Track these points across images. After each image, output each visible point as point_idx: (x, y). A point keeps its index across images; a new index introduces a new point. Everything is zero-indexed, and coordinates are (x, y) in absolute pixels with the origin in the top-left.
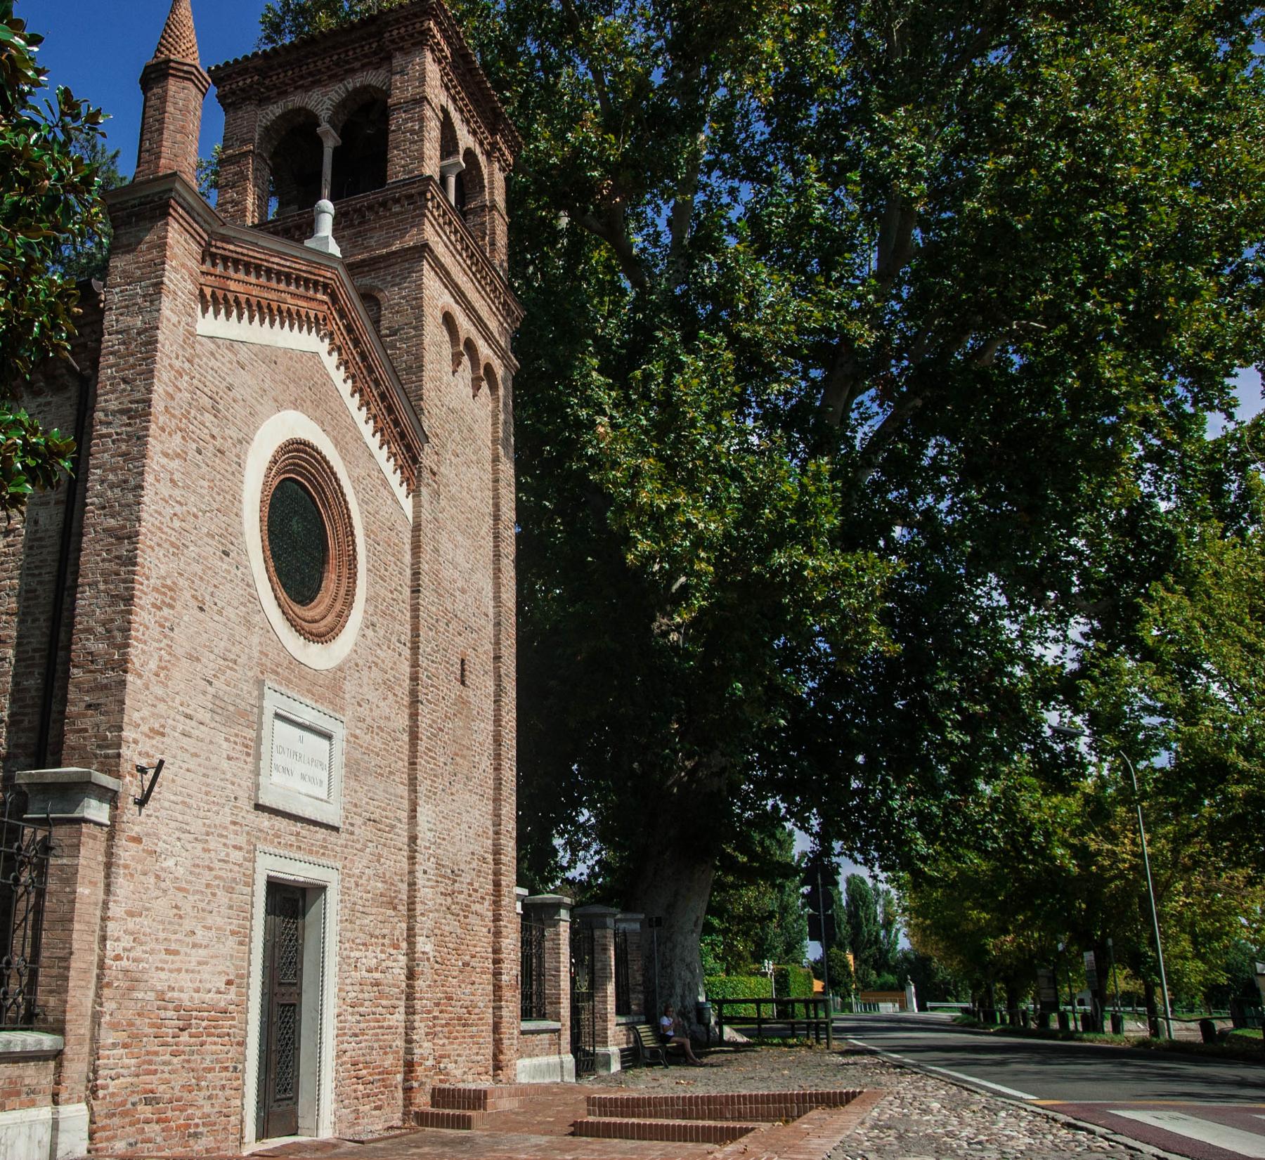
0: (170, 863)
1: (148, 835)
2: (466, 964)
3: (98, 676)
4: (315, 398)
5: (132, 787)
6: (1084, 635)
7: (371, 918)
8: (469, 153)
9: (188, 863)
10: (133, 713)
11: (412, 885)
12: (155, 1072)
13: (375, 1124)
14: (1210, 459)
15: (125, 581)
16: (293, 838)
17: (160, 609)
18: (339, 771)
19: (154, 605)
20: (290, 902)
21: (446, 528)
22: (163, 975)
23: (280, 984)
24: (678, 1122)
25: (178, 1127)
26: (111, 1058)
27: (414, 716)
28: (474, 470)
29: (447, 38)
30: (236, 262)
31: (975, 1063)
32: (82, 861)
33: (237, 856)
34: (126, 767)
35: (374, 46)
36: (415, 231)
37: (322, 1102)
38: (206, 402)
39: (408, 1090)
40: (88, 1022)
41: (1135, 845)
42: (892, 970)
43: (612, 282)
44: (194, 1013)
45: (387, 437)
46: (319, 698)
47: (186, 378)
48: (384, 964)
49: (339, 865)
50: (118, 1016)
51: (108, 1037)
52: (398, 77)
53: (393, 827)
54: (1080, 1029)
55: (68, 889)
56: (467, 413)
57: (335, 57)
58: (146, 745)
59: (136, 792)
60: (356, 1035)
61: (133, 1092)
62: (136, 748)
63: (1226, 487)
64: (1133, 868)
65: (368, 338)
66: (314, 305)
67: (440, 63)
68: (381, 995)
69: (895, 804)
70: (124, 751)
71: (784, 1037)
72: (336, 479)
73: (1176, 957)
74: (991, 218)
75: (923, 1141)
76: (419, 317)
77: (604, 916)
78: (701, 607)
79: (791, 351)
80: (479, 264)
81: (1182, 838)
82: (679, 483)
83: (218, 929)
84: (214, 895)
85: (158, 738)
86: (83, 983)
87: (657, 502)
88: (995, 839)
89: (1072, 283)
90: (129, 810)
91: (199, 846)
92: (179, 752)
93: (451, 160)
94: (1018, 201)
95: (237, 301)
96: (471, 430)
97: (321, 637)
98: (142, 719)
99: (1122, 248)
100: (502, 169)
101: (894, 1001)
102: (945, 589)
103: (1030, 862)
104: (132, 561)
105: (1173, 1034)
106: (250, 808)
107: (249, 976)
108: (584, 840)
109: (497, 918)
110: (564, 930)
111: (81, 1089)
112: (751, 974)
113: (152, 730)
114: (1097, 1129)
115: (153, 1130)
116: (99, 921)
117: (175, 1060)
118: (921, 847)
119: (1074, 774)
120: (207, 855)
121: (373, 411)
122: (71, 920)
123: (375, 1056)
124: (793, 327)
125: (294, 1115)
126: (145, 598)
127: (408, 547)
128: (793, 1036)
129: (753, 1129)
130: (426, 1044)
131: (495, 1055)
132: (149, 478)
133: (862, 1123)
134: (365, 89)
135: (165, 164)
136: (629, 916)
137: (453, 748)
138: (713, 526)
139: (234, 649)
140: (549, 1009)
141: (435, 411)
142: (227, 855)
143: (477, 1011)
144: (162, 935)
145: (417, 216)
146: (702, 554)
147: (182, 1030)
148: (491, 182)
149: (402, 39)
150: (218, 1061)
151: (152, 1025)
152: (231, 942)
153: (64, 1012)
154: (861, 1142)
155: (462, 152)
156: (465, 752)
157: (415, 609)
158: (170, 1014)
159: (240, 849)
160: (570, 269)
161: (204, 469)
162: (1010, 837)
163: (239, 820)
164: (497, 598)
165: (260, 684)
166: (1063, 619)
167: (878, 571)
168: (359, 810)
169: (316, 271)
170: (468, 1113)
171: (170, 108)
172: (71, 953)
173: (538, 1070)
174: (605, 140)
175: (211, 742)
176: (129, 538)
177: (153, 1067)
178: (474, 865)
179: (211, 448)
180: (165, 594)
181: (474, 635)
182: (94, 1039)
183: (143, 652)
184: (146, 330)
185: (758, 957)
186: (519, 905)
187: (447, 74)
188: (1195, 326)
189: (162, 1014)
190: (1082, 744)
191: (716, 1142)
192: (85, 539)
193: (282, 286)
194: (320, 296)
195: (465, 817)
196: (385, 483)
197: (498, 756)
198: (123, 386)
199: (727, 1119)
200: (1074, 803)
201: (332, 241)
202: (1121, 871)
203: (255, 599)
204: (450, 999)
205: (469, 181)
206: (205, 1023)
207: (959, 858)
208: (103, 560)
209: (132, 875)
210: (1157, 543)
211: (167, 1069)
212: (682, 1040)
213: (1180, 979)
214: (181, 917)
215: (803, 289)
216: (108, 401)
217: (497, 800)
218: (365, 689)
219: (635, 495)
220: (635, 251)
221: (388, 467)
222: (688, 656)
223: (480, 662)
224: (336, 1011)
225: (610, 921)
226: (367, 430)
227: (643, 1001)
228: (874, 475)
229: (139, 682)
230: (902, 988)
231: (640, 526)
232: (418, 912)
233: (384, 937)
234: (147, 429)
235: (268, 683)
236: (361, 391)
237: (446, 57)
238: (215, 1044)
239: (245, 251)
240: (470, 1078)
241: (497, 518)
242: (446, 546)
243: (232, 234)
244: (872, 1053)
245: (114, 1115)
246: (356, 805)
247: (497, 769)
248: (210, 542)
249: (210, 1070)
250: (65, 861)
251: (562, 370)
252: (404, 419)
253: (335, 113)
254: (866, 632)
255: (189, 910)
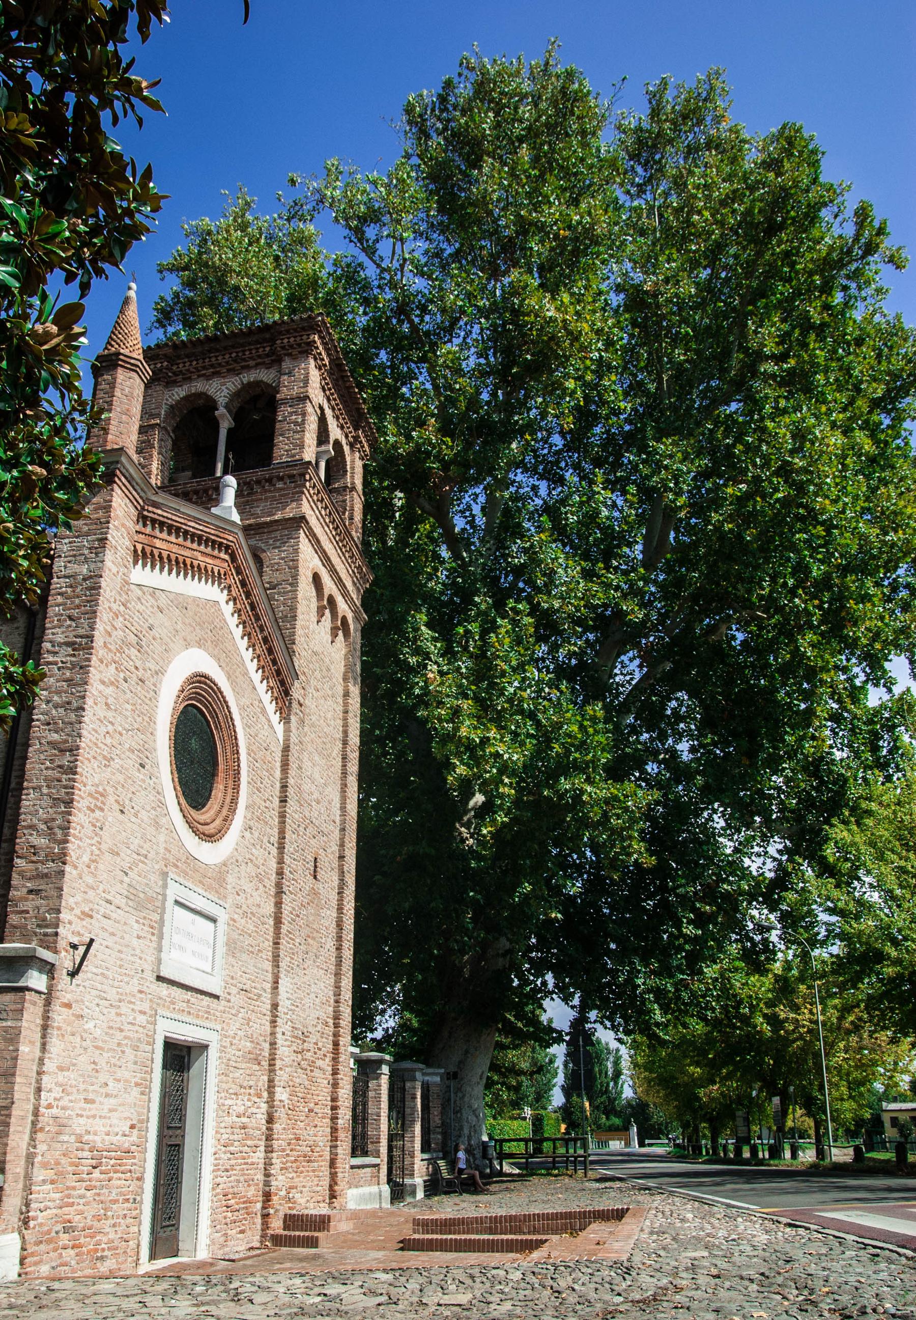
0: (90, 1025)
1: (77, 1001)
2: (310, 1111)
3: (39, 865)
4: (213, 640)
5: (65, 960)
6: (779, 851)
7: (241, 1071)
8: (337, 443)
9: (105, 1025)
10: (68, 900)
11: (273, 1044)
12: (72, 1205)
13: (239, 1246)
14: (870, 722)
15: (66, 787)
16: (185, 1005)
17: (93, 811)
18: (221, 949)
19: (89, 808)
20: (180, 1057)
21: (307, 751)
22: (82, 1121)
23: (169, 1128)
24: (486, 1237)
25: (89, 1252)
26: (44, 1194)
27: (278, 904)
28: (330, 703)
29: (327, 350)
30: (162, 524)
31: (701, 1184)
32: (24, 1024)
33: (142, 1019)
34: (62, 944)
35: (268, 349)
36: (294, 505)
37: (200, 1227)
38: (132, 639)
39: (265, 1216)
40: (23, 1162)
41: (812, 1013)
42: (618, 1114)
43: (434, 552)
44: (105, 1153)
45: (267, 674)
46: (209, 888)
47: (121, 619)
48: (250, 1111)
49: (219, 1027)
50: (48, 1157)
51: (39, 1174)
52: (286, 377)
53: (259, 996)
54: (767, 1156)
55: (11, 1048)
56: (326, 654)
57: (234, 355)
58: (78, 926)
59: (69, 965)
60: (227, 1171)
61: (57, 1222)
62: (70, 929)
63: (881, 743)
64: (810, 1031)
65: (257, 592)
66: (217, 562)
67: (320, 369)
68: (248, 1137)
69: (639, 981)
70: (60, 930)
71: (547, 1169)
72: (228, 707)
73: (837, 1099)
74: (731, 531)
75: (693, 1241)
76: (295, 577)
77: (414, 1070)
78: (503, 822)
79: (579, 622)
80: (341, 533)
81: (846, 1010)
82: (491, 720)
83: (126, 1081)
84: (123, 1052)
85: (88, 919)
86: (20, 1129)
87: (472, 736)
88: (713, 1010)
89: (785, 584)
90: (63, 979)
91: (113, 1011)
92: (101, 932)
93: (323, 448)
94: (749, 519)
95: (160, 556)
96: (328, 670)
97: (210, 837)
98: (76, 903)
99: (819, 560)
100: (362, 458)
101: (620, 1139)
102: (680, 812)
103: (738, 1028)
104: (72, 770)
105: (834, 1159)
106: (153, 979)
107: (148, 1121)
108: (381, 1006)
109: (335, 1072)
110: (384, 1081)
111: (15, 1221)
112: (513, 1118)
113: (83, 913)
114: (812, 1226)
115: (69, 1255)
116: (35, 1075)
117: (88, 1194)
118: (658, 1016)
119: (767, 959)
120: (119, 1019)
121: (258, 652)
122: (14, 1075)
123: (241, 1188)
124: (582, 603)
125: (175, 1239)
126: (82, 802)
127: (278, 764)
128: (555, 1168)
129: (546, 1241)
130: (280, 1178)
131: (331, 1186)
132: (89, 701)
133: (642, 1230)
134: (258, 383)
135: (113, 440)
136: (431, 1070)
137: (307, 931)
138: (515, 757)
139: (145, 846)
140: (370, 1147)
141: (303, 653)
142: (135, 1019)
143: (318, 1149)
144: (82, 1087)
145: (297, 493)
146: (506, 780)
147: (94, 1168)
148: (353, 468)
149: (291, 347)
150: (122, 1194)
151: (72, 1164)
152: (135, 1092)
153: (5, 1153)
154: (649, 1244)
155: (332, 442)
156: (315, 934)
157: (282, 816)
158: (86, 1154)
159: (145, 1013)
160: (402, 541)
161: (129, 695)
162: (725, 1008)
163: (145, 989)
164: (343, 808)
165: (165, 875)
166: (765, 838)
167: (638, 796)
168: (234, 982)
169: (222, 535)
170: (316, 1234)
171: (118, 393)
172: (13, 1103)
173: (362, 1198)
174: (444, 443)
175: (125, 923)
176: (71, 751)
177: (71, 1200)
178: (319, 1028)
179: (135, 678)
180: (97, 799)
181: (325, 838)
182: (28, 1177)
183: (79, 847)
184: (91, 577)
185: (516, 1105)
186: (352, 1061)
187: (325, 379)
188: (868, 623)
189: (80, 1154)
190: (774, 936)
191: (517, 1252)
192: (31, 749)
193: (195, 546)
194: (223, 555)
195: (314, 988)
196: (264, 711)
197: (339, 938)
198: (69, 622)
199: (524, 1233)
200: (768, 981)
201: (234, 510)
202: (801, 1034)
203: (162, 804)
204: (298, 1139)
205: (336, 466)
206: (112, 1162)
207: (685, 1026)
208: (47, 768)
209: (63, 1035)
210: (834, 784)
211: (82, 1201)
212: (472, 1172)
213: (838, 1116)
214: (97, 1071)
215: (588, 575)
216: (56, 633)
217: (338, 974)
218: (243, 880)
219: (456, 729)
220: (457, 530)
221: (267, 698)
222: (479, 857)
223: (329, 861)
224: (213, 1150)
225: (418, 1075)
226: (252, 666)
227: (440, 1143)
228: (630, 720)
229: (74, 872)
230: (626, 1128)
231: (458, 755)
232: (277, 1067)
233: (250, 1087)
234: (89, 660)
235: (171, 875)
236: (249, 634)
237: (325, 365)
238: (120, 1179)
239: (170, 516)
240: (312, 1205)
241: (345, 743)
242: (307, 764)
243: (160, 501)
244: (620, 1179)
245: (41, 1242)
246: (232, 978)
247: (339, 949)
248: (131, 756)
249: (115, 1202)
250: (9, 1023)
251: (397, 624)
252: (281, 660)
253: (231, 400)
254: (630, 846)
255: (104, 1065)
